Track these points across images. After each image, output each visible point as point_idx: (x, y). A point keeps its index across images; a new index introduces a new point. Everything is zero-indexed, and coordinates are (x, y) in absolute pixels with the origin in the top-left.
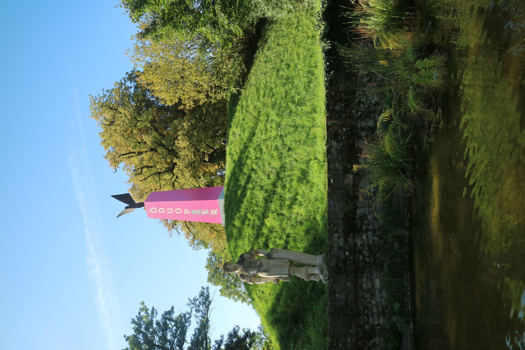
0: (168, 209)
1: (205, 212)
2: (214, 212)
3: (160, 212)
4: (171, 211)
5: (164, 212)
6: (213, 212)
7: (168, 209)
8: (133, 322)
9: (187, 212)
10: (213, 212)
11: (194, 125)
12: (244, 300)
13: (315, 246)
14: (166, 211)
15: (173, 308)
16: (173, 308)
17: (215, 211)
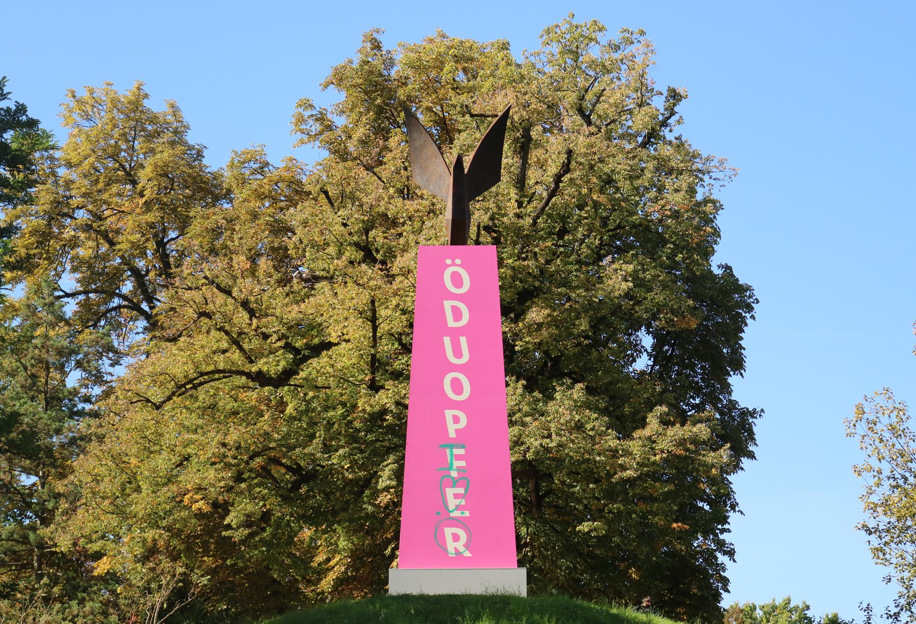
0: (463, 340)
1: (453, 498)
2: (456, 541)
3: (448, 305)
4: (458, 353)
5: (451, 323)
6: (456, 538)
7: (463, 340)
8: (751, 456)
9: (455, 422)
10: (456, 538)
11: (327, 520)
12: (400, 513)
13: (229, 511)
14: (455, 334)
15: (734, 561)
16: (734, 561)
17: (460, 545)
